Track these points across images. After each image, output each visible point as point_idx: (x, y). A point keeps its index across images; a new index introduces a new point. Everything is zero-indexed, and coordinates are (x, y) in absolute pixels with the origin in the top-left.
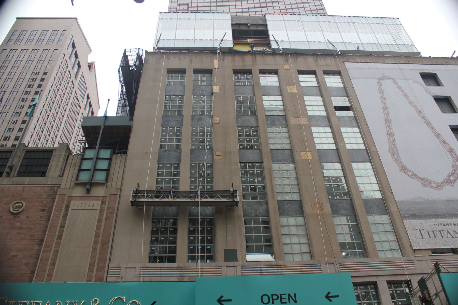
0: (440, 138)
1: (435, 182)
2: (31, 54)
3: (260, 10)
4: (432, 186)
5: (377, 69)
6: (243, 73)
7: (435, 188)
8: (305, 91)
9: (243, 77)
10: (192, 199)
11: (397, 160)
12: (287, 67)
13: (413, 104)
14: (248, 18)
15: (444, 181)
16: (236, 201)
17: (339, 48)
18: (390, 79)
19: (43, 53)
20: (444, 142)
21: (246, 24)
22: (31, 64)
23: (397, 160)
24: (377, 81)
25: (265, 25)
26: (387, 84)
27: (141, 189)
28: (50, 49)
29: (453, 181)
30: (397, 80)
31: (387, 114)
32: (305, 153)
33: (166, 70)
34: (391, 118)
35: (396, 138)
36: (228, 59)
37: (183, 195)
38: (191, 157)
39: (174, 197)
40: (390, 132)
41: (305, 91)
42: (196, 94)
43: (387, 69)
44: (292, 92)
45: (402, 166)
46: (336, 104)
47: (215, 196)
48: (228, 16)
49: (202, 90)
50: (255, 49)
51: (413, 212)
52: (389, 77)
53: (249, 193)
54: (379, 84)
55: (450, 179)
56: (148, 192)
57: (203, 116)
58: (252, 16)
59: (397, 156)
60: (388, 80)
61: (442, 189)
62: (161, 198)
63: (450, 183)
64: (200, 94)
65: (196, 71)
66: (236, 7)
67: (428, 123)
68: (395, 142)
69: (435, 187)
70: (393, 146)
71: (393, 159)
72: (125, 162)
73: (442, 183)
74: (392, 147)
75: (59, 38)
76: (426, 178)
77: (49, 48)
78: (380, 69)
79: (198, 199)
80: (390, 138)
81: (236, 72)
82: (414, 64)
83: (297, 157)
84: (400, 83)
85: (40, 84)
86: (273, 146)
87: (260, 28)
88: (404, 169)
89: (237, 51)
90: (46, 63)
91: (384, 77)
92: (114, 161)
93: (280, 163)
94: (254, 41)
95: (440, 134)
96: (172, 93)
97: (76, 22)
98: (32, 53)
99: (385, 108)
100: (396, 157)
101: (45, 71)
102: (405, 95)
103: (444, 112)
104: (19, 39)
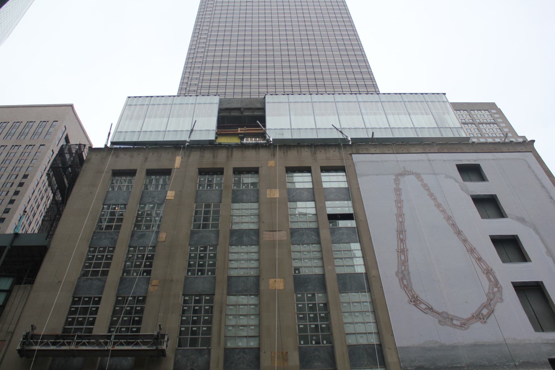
0: (475, 254)
1: (460, 318)
2: (10, 152)
3: (314, 83)
4: (455, 325)
5: (397, 161)
6: (212, 173)
7: (458, 327)
8: (292, 195)
9: (203, 179)
10: (101, 347)
11: (407, 287)
12: (271, 163)
13: (441, 207)
14: (242, 100)
15: (473, 316)
16: (161, 349)
17: (350, 136)
18: (413, 174)
19: (25, 150)
20: (480, 259)
21: (239, 109)
22: (8, 165)
23: (407, 288)
24: (394, 177)
25: (263, 109)
26: (409, 182)
27: (36, 332)
28: (34, 145)
29: (485, 316)
30: (423, 176)
31: (401, 222)
32: (275, 281)
33: (111, 172)
34: (406, 229)
35: (409, 257)
36: (195, 156)
37: (91, 341)
38: (120, 288)
39: (78, 343)
40: (402, 247)
41: (292, 195)
42: (144, 202)
43: (411, 161)
44: (272, 197)
45: (413, 297)
46: (330, 211)
47: (133, 342)
48: (216, 99)
49: (152, 198)
50: (245, 141)
51: (420, 363)
52: (413, 172)
53: (308, 335)
54: (397, 181)
55: (482, 313)
56: (44, 337)
57: (147, 233)
58: (244, 98)
59: (407, 282)
60: (410, 176)
61: (468, 328)
62: (60, 345)
63: (480, 319)
64: (149, 202)
65: (150, 173)
66: (283, 80)
67: (459, 233)
68: (407, 261)
69: (457, 326)
70: (403, 267)
71: (401, 286)
72: (29, 295)
73: (469, 319)
74: (402, 269)
75: (48, 131)
76: (446, 312)
77: (33, 144)
78: (400, 161)
79: (110, 346)
80: (400, 256)
81: (202, 172)
82: (450, 153)
83: (262, 287)
84: (428, 179)
85: (17, 190)
86: (234, 271)
87: (256, 113)
88: (415, 301)
89: (220, 144)
90: (27, 163)
91: (405, 173)
92: (14, 294)
93: (239, 295)
94: (246, 131)
95: (475, 249)
96: (113, 202)
97: (72, 110)
98: (11, 150)
99: (400, 215)
100: (405, 282)
101: (26, 174)
102: (431, 195)
103: (484, 216)
104: (11, 132)
